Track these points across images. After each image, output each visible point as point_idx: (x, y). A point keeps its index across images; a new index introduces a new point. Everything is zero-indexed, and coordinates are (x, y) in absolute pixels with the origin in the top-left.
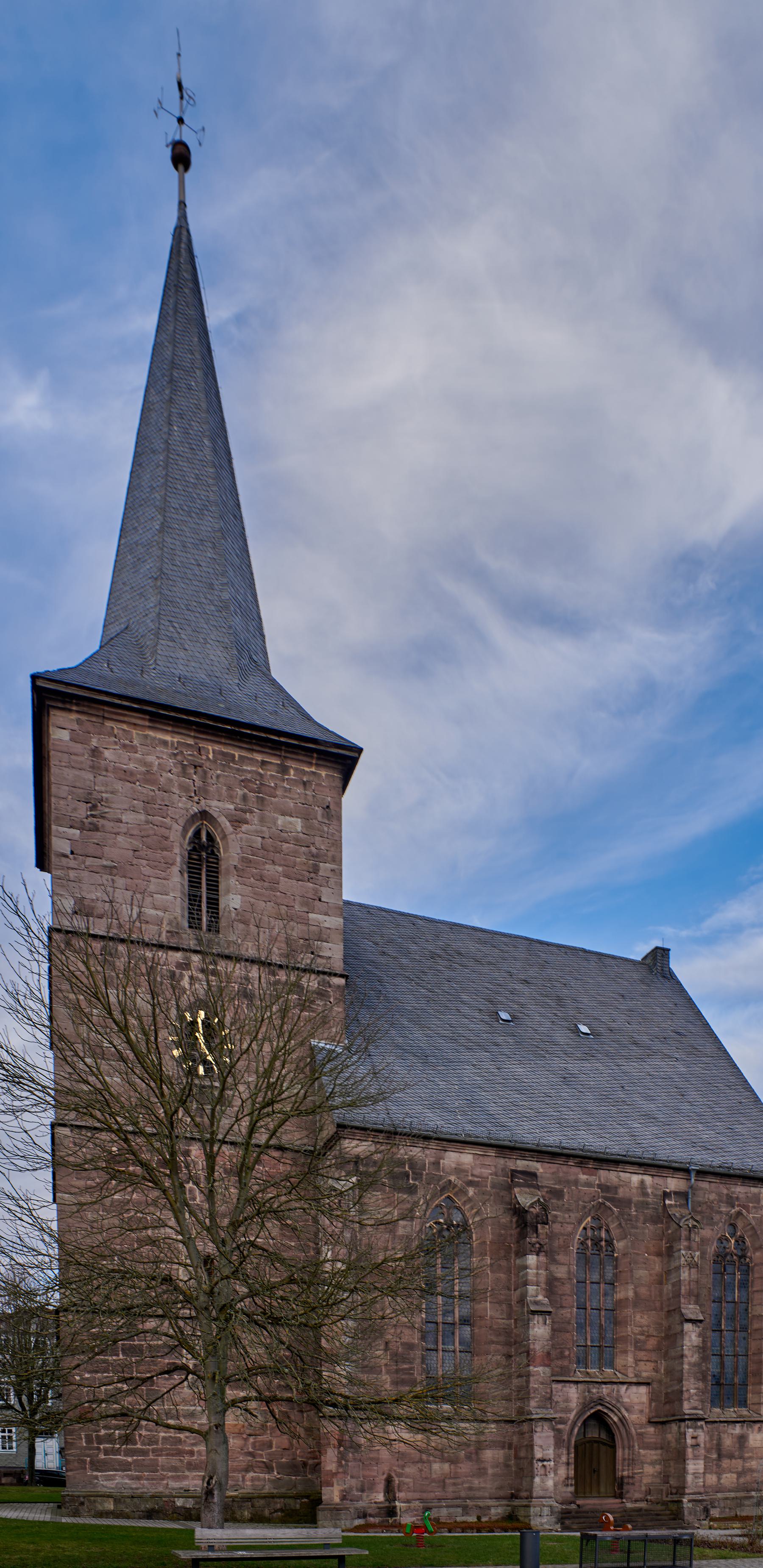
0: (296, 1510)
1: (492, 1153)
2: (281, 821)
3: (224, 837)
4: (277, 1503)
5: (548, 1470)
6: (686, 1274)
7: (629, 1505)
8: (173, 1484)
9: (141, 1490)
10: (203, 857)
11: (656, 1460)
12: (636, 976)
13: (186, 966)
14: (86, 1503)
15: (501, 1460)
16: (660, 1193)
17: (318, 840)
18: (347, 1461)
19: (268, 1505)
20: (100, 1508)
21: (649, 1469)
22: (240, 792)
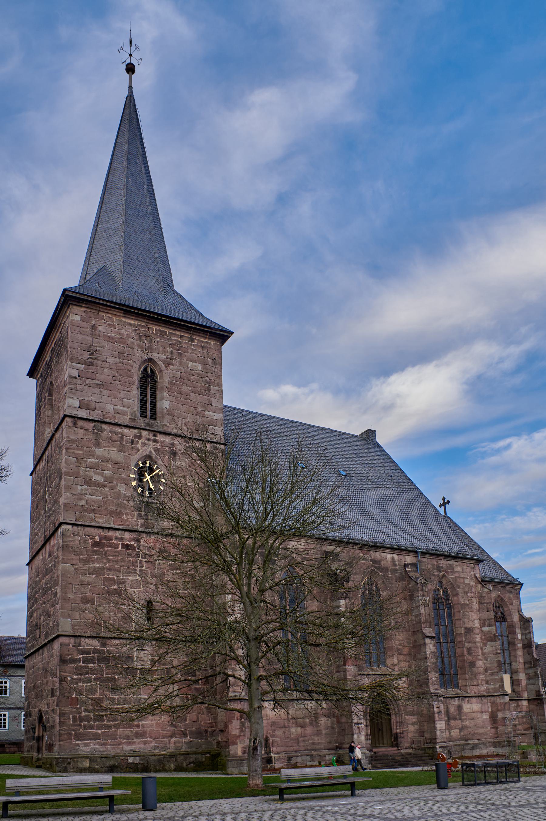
0: (203, 762)
1: (314, 542)
2: (190, 364)
3: (161, 371)
4: (190, 758)
5: (361, 730)
6: (423, 610)
7: (403, 751)
8: (127, 748)
9: (105, 753)
10: (149, 380)
11: (415, 722)
12: (360, 444)
13: (140, 437)
14: (72, 763)
15: (329, 725)
16: (402, 564)
17: (210, 375)
18: (245, 728)
19: (186, 759)
20: (81, 766)
21: (411, 728)
22: (169, 350)
